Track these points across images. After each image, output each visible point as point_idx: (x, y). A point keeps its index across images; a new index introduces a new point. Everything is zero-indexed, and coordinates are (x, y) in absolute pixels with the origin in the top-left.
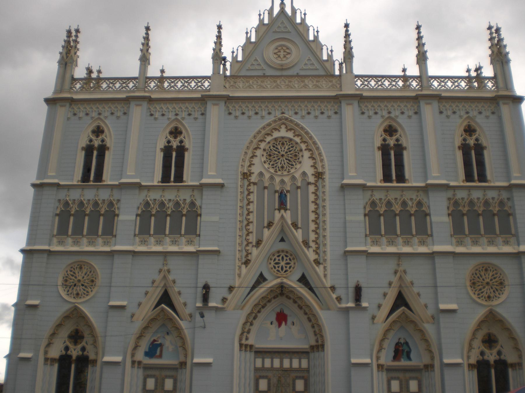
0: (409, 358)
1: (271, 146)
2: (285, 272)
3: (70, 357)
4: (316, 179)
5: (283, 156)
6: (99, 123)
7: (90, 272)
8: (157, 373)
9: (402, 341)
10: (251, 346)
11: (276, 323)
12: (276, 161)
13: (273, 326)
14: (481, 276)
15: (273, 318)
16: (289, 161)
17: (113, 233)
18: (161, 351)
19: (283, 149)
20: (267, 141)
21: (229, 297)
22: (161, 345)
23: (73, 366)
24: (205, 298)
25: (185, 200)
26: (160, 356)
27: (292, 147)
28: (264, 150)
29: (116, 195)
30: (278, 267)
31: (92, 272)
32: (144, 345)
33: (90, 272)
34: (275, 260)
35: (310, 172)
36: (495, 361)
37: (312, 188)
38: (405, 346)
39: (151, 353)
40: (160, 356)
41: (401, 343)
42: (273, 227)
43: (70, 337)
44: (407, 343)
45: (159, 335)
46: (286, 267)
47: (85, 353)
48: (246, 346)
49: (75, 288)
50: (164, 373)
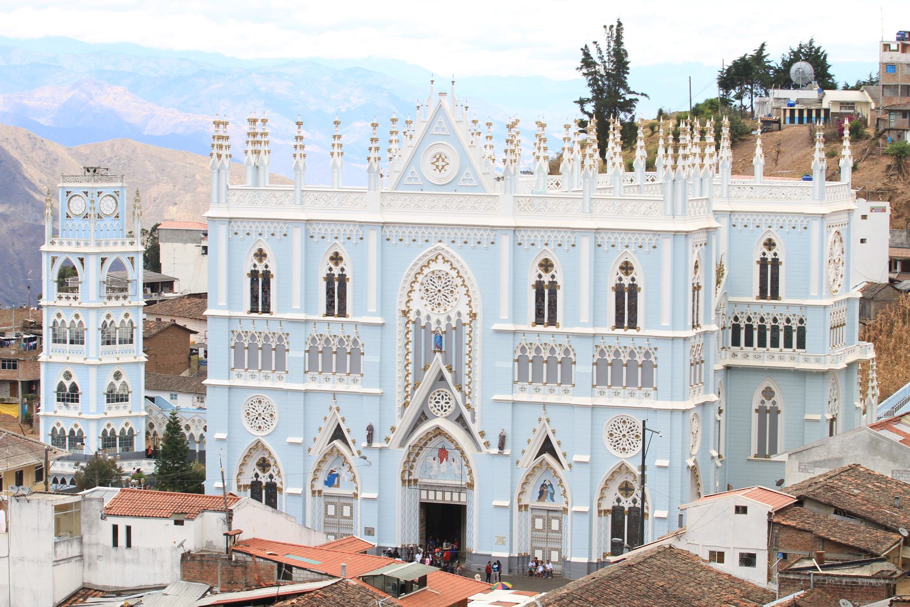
0: (553, 500)
1: (429, 280)
2: (445, 411)
3: (261, 483)
4: (471, 319)
5: (439, 291)
6: (260, 245)
7: (252, 404)
8: (336, 500)
9: (547, 483)
10: (416, 481)
11: (438, 459)
12: (433, 296)
13: (436, 461)
14: (619, 428)
15: (436, 453)
16: (446, 297)
17: (572, 382)
18: (338, 481)
19: (440, 283)
20: (425, 274)
21: (392, 436)
22: (337, 475)
23: (264, 492)
24: (370, 438)
25: (349, 337)
26: (338, 486)
27: (449, 281)
28: (422, 284)
29: (287, 328)
30: (439, 406)
31: (253, 403)
32: (323, 476)
33: (252, 404)
34: (435, 399)
35: (465, 311)
36: (630, 508)
37: (467, 329)
38: (549, 488)
39: (332, 480)
40: (338, 486)
41: (546, 485)
42: (429, 369)
43: (258, 465)
44: (551, 485)
45: (336, 466)
46: (446, 406)
47: (273, 480)
48: (409, 481)
49: (257, 421)
50: (342, 501)
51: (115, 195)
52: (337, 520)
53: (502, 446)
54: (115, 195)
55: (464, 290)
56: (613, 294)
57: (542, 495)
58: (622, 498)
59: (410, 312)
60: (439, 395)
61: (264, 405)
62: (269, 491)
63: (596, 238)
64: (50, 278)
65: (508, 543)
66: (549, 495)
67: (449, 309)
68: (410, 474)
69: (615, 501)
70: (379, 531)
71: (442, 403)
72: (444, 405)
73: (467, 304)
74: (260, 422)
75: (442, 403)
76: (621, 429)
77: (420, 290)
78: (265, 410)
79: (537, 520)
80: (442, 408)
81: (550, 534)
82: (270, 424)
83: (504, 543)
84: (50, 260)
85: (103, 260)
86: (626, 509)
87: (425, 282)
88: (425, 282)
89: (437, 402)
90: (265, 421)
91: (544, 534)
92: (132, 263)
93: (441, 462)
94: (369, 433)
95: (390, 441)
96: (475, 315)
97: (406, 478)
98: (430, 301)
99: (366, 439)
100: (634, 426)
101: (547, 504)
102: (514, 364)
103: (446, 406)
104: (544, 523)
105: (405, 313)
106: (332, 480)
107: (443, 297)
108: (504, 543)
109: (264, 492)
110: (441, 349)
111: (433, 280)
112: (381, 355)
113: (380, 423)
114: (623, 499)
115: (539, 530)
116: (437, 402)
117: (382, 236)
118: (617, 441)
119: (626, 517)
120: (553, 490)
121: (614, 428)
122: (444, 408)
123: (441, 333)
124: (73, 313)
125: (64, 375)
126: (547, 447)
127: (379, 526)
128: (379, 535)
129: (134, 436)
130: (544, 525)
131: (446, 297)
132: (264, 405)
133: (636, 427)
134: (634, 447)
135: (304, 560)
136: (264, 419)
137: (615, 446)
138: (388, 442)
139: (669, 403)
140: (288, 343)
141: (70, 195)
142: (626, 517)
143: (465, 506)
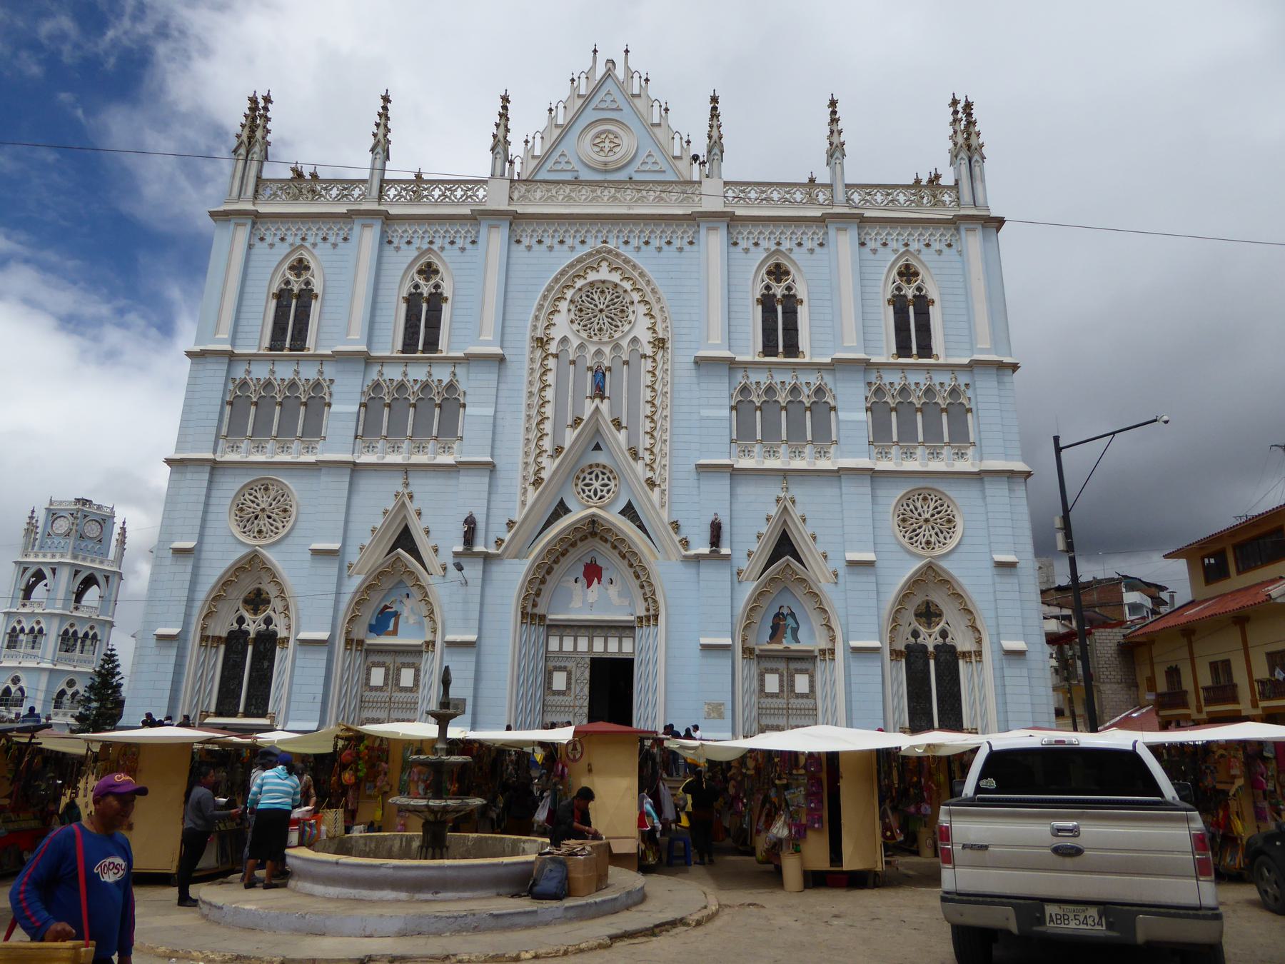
1: (584, 295)
2: (600, 498)
7: (250, 494)
9: (785, 611)
10: (543, 618)
11: (583, 581)
16: (612, 319)
18: (396, 625)
23: (250, 648)
26: (395, 632)
27: (618, 297)
29: (329, 371)
32: (368, 616)
35: (645, 337)
40: (395, 632)
41: (783, 614)
44: (793, 615)
45: (393, 599)
50: (400, 659)
51: (102, 522)
52: (386, 694)
53: (716, 540)
54: (102, 522)
55: (642, 309)
56: (890, 310)
57: (776, 634)
58: (922, 630)
59: (594, 271)
60: (591, 473)
61: (272, 494)
62: (262, 648)
63: (859, 234)
64: (18, 587)
65: (728, 714)
66: (789, 631)
67: (617, 335)
68: (535, 605)
69: (910, 636)
70: (475, 706)
71: (597, 485)
72: (600, 482)
73: (648, 329)
74: (263, 523)
75: (597, 485)
76: (920, 510)
77: (569, 310)
78: (274, 503)
79: (767, 676)
80: (596, 494)
81: (792, 701)
82: (280, 525)
83: (721, 716)
84: (22, 569)
85: (77, 573)
86: (931, 649)
87: (577, 298)
88: (577, 298)
89: (587, 485)
90: (271, 521)
91: (781, 702)
92: (107, 581)
93: (588, 586)
94: (469, 528)
95: (504, 545)
96: (662, 341)
97: (529, 609)
98: (586, 326)
99: (462, 540)
100: (942, 505)
101: (787, 643)
102: (731, 413)
103: (590, 491)
104: (781, 681)
105: (541, 342)
106: (385, 620)
107: (606, 319)
108: (721, 716)
109: (250, 648)
110: (604, 392)
111: (591, 296)
112: (496, 407)
113: (488, 516)
114: (923, 630)
115: (772, 695)
116: (587, 485)
117: (510, 237)
118: (914, 530)
119: (932, 663)
120: (797, 623)
121: (908, 509)
122: (599, 494)
123: (604, 369)
124: (34, 620)
125: (13, 680)
126: (784, 546)
127: (475, 697)
128: (474, 714)
129: (24, 590)
130: (781, 686)
131: (612, 319)
132: (272, 494)
133: (945, 505)
134: (945, 538)
135: (624, 399)
136: (269, 517)
137: (911, 538)
138: (500, 545)
139: (1004, 462)
140: (331, 394)
141: (55, 516)
142: (932, 663)
143: (631, 662)
